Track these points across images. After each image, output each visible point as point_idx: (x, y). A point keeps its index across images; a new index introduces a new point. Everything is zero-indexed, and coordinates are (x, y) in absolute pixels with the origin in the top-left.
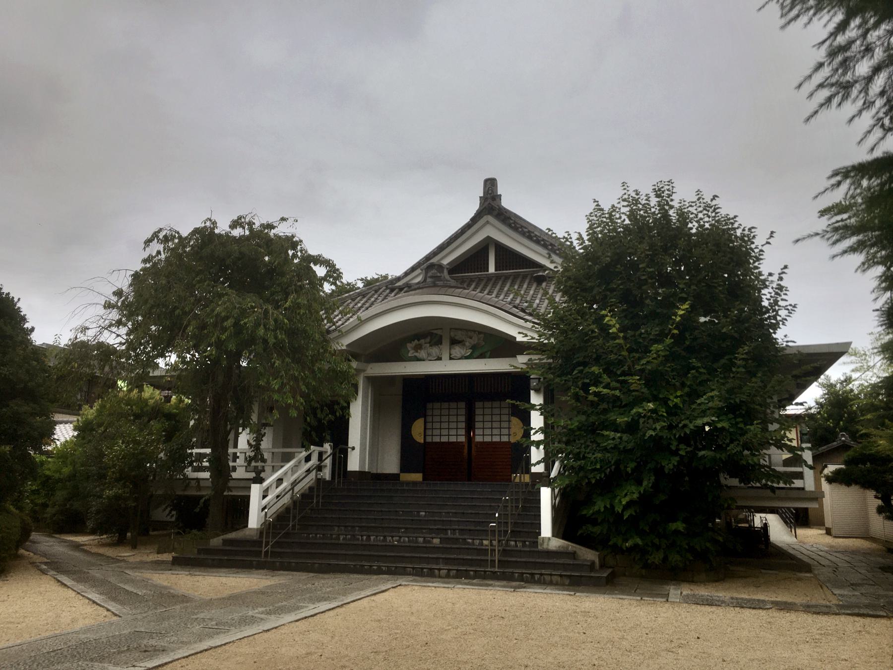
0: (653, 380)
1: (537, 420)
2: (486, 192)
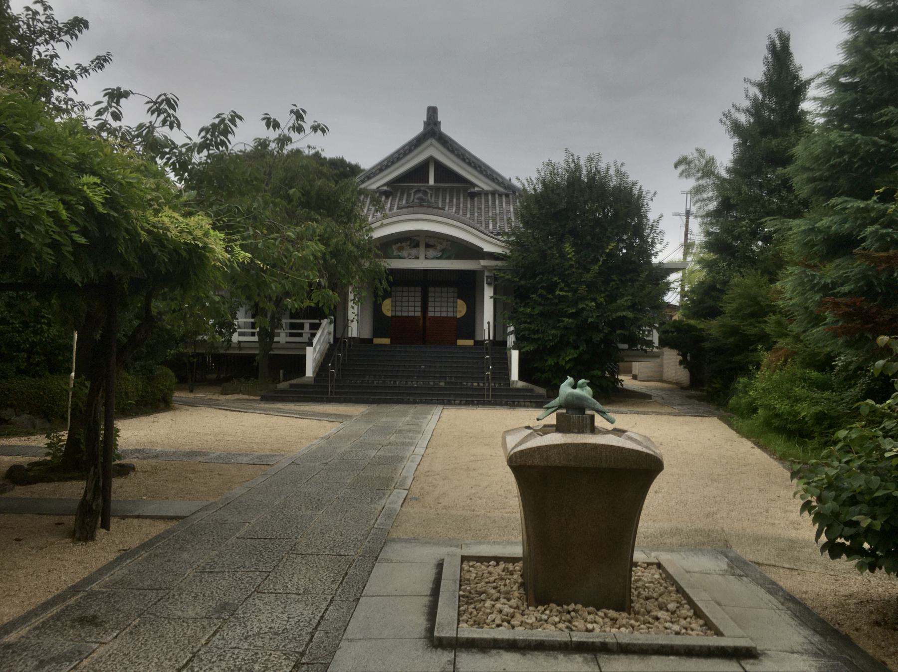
2: (429, 118)
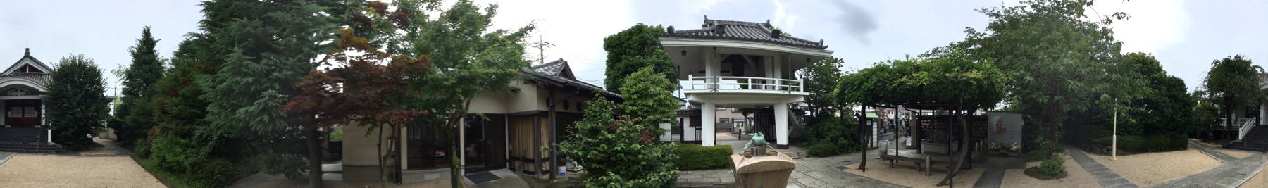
0: (79, 103)
1: (43, 111)
